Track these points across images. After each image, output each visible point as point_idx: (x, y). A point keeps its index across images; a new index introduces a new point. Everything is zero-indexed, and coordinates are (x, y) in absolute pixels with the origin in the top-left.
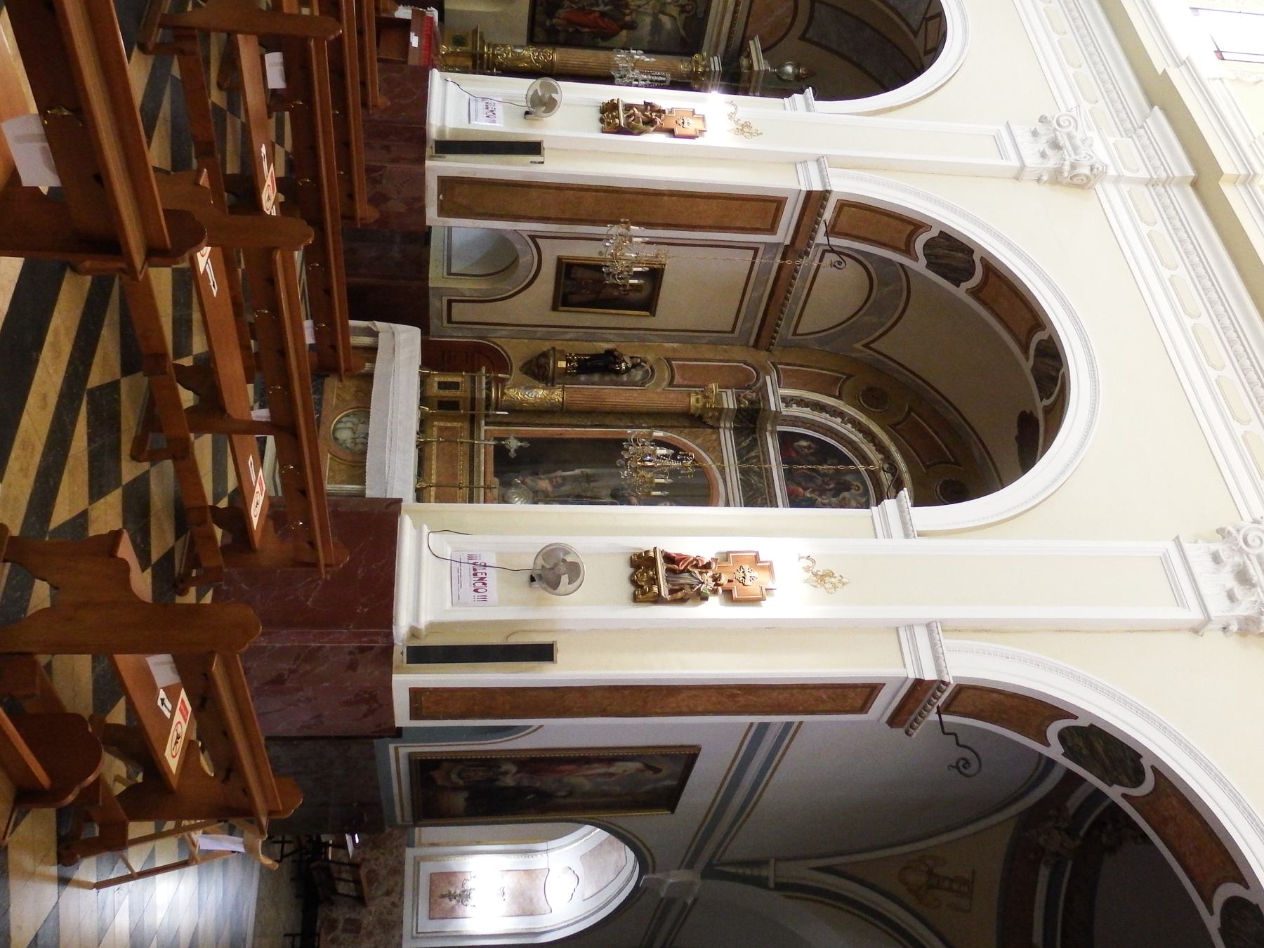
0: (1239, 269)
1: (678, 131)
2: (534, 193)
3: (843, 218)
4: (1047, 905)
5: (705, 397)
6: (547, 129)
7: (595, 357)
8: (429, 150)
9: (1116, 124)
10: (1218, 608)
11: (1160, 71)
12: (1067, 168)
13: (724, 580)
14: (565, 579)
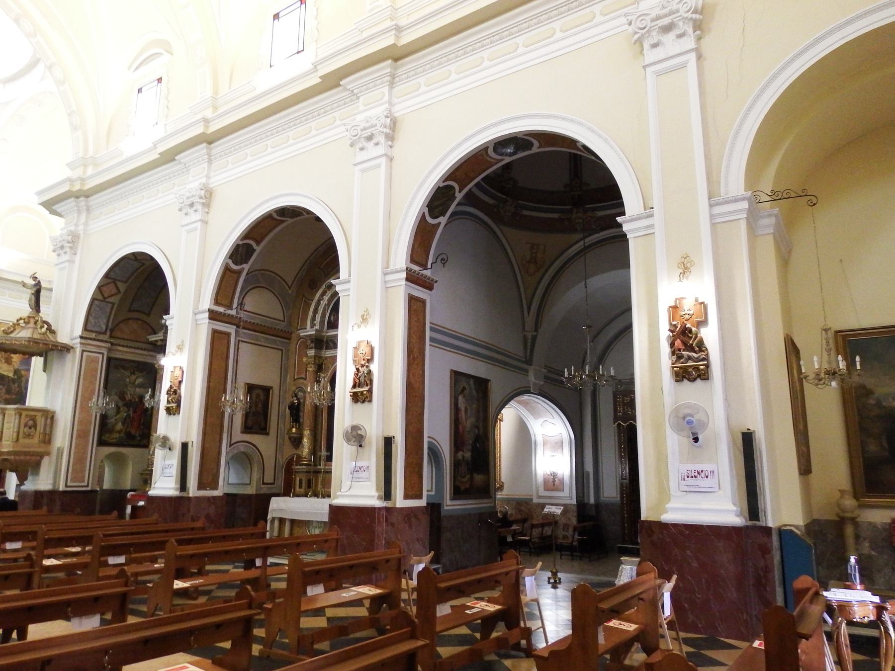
0: (275, 113)
2: (207, 445)
3: (224, 302)
4: (545, 212)
5: (309, 364)
6: (176, 440)
7: (291, 414)
8: (184, 494)
9: (548, 24)
10: (381, 150)
12: (201, 201)
13: (363, 362)
14: (359, 432)
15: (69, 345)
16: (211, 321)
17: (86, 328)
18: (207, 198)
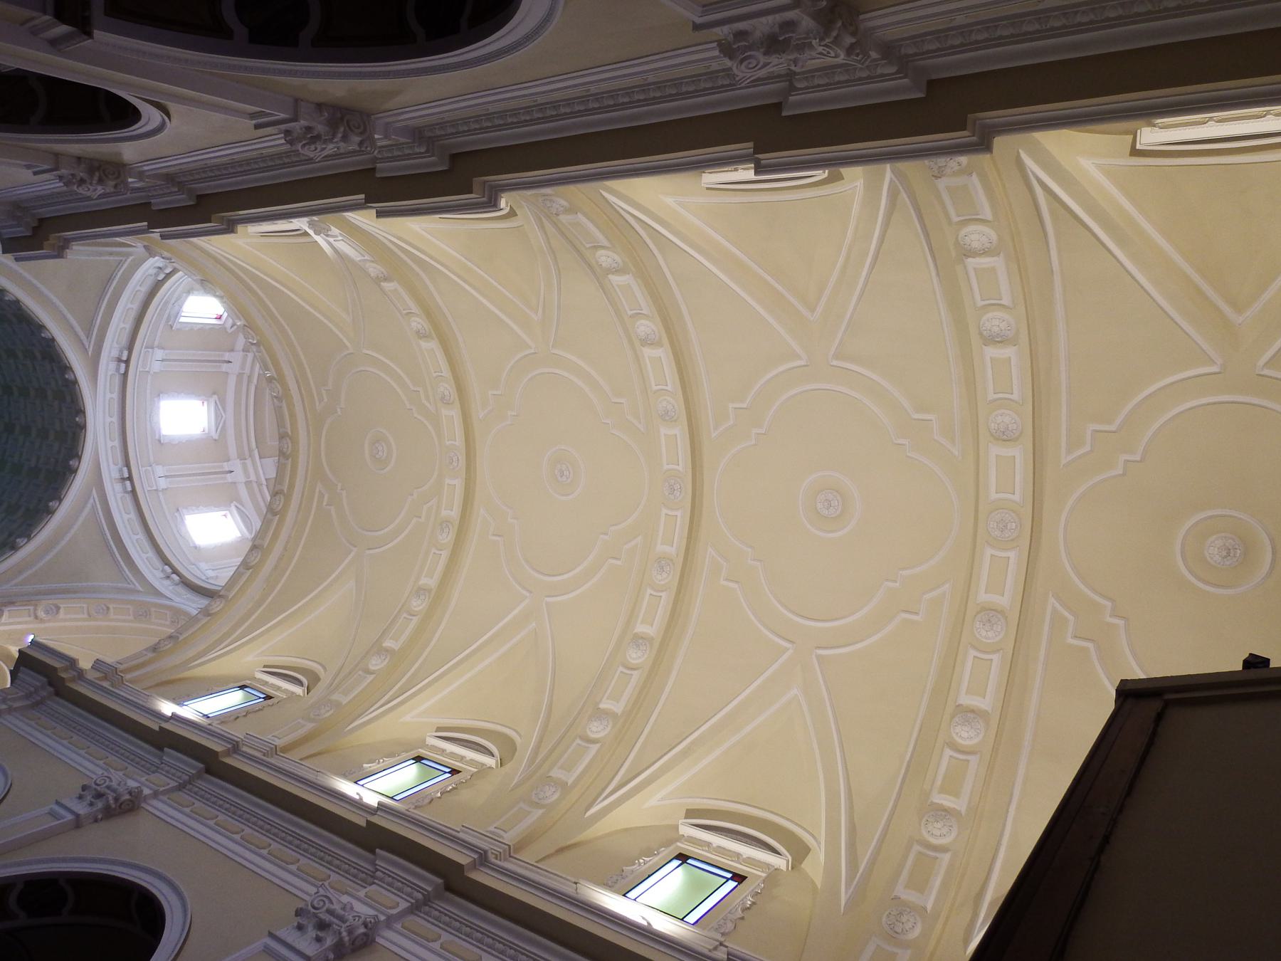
11: (157, 729)
18: (120, 807)
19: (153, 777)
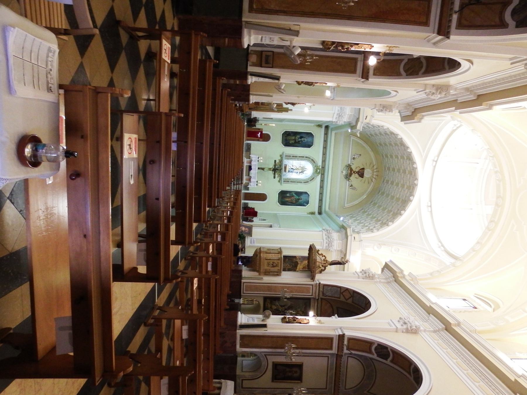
1: (302, 322)
8: (238, 328)
12: (409, 327)
15: (314, 279)
16: (338, 336)
17: (325, 285)
19: (424, 323)
